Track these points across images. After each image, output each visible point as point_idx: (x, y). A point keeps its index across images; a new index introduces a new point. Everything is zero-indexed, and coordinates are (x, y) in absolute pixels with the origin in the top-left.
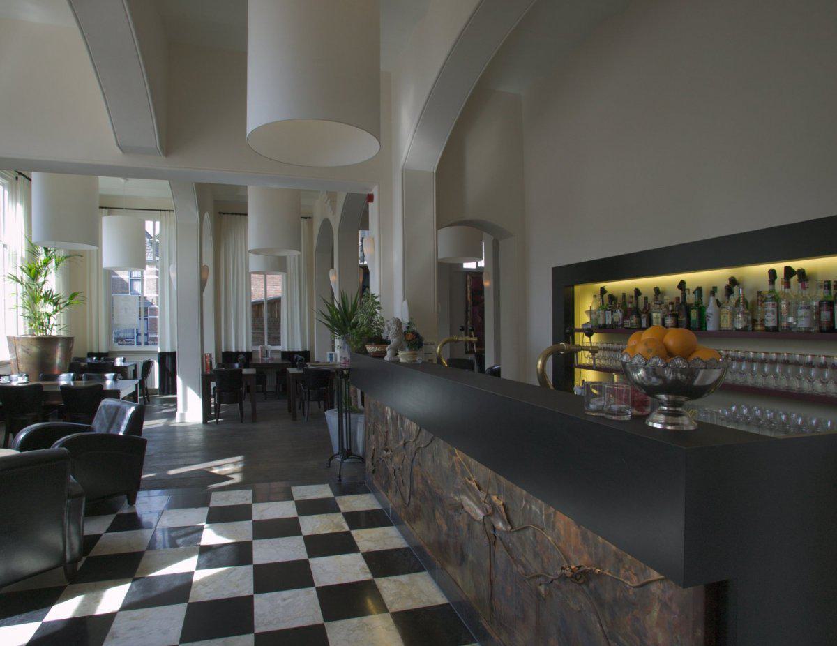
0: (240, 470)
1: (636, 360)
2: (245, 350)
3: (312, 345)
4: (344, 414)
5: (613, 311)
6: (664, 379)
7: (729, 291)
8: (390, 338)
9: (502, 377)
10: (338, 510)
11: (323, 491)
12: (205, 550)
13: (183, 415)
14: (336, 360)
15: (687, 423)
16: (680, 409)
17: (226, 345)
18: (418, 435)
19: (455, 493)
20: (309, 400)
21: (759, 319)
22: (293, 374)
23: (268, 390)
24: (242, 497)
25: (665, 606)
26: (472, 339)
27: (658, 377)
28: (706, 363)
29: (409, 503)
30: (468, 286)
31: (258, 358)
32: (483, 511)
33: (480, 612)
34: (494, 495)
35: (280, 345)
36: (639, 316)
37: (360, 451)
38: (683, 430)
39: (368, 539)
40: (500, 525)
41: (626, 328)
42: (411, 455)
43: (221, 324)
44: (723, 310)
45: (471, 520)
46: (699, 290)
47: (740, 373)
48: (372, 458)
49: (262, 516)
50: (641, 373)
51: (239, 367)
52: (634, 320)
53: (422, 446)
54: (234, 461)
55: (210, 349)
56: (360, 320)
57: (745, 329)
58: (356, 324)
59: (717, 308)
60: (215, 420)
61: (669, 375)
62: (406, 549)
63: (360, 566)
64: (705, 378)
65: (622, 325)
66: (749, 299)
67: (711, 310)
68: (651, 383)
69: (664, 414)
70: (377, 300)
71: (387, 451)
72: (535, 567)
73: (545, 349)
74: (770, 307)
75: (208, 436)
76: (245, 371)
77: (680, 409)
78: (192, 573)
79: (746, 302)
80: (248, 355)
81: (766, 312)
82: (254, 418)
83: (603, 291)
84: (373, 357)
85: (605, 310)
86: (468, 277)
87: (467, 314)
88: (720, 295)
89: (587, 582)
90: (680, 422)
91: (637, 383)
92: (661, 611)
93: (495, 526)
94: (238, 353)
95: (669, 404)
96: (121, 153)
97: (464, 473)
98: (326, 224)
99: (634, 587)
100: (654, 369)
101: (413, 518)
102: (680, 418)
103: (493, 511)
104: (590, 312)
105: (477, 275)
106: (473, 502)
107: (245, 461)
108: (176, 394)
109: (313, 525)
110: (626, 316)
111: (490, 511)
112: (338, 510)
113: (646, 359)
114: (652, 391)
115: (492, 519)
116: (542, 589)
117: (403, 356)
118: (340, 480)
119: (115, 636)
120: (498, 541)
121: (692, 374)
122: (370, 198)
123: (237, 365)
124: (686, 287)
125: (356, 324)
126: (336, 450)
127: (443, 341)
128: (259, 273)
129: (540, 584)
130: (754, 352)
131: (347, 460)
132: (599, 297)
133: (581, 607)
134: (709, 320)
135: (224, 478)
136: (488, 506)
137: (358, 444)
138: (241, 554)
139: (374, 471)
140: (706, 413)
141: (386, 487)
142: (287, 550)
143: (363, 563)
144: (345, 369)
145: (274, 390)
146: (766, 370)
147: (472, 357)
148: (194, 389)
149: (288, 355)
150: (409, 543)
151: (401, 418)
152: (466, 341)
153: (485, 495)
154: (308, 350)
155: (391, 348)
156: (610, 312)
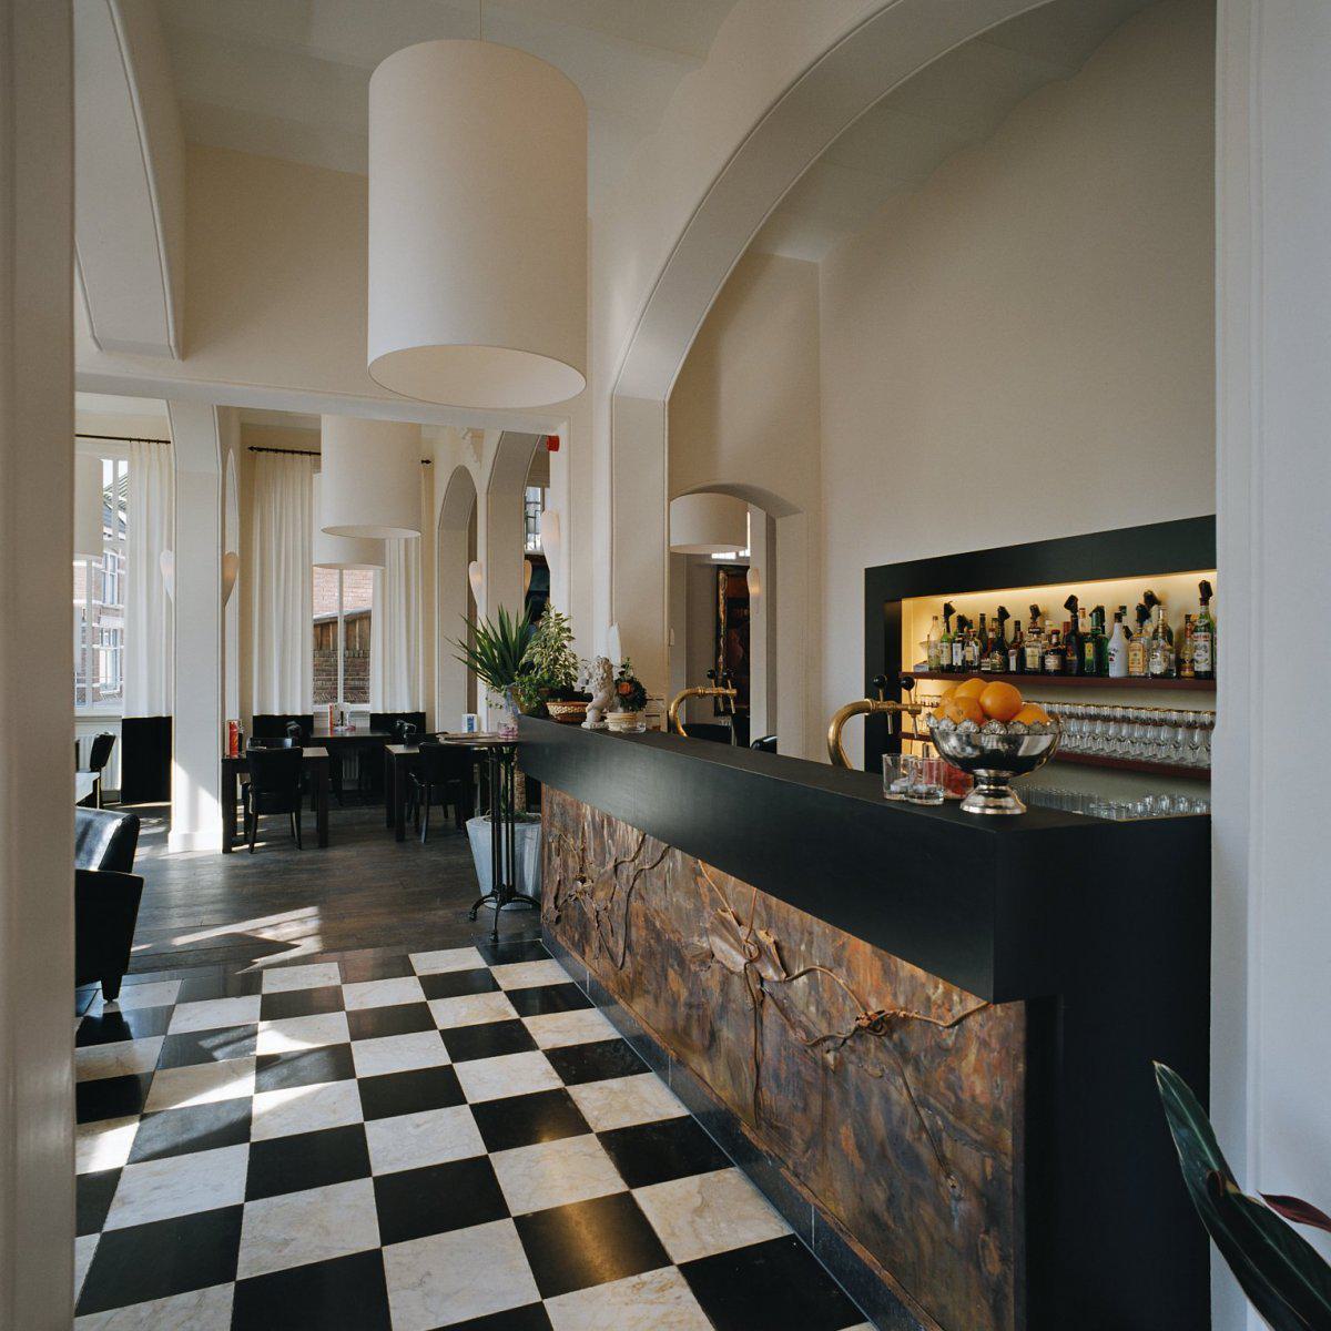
0: (315, 931)
1: (943, 726)
2: (299, 714)
3: (430, 701)
4: (503, 825)
5: (964, 644)
6: (982, 749)
7: (1143, 614)
8: (592, 691)
9: (779, 753)
10: (497, 988)
11: (469, 959)
12: (265, 1064)
13: (188, 838)
14: (479, 727)
15: (1013, 805)
16: (1004, 788)
17: (262, 703)
18: (639, 849)
19: (701, 936)
20: (430, 804)
21: (1187, 658)
22: (397, 755)
23: (346, 787)
24: (323, 975)
25: (984, 1044)
26: (728, 692)
27: (974, 747)
28: (1029, 728)
29: (623, 964)
30: (721, 592)
31: (324, 728)
32: (744, 955)
33: (740, 1115)
34: (761, 929)
35: (366, 701)
36: (1005, 653)
37: (530, 891)
38: (1007, 815)
39: (553, 1030)
40: (770, 973)
41: (985, 672)
42: (628, 882)
43: (252, 666)
44: (1133, 644)
45: (727, 975)
46: (1100, 611)
47: (1145, 744)
48: (556, 898)
49: (362, 1003)
50: (953, 741)
51: (294, 743)
52: (996, 658)
53: (647, 867)
54: (299, 916)
55: (233, 715)
56: (536, 660)
57: (1166, 675)
58: (530, 665)
59: (1125, 640)
60: (247, 846)
61: (991, 743)
62: (618, 1041)
63: (541, 1070)
64: (1032, 746)
65: (979, 667)
66: (1175, 626)
67: (1115, 643)
68: (965, 754)
69: (985, 795)
70: (565, 625)
71: (583, 881)
72: (822, 1029)
73: (841, 708)
74: (1201, 640)
75: (235, 877)
76: (308, 752)
77: (1004, 788)
78: (250, 1099)
79: (1168, 633)
80: (306, 722)
81: (1196, 648)
82: (323, 839)
83: (948, 610)
84: (560, 722)
85: (952, 641)
86: (722, 575)
87: (718, 642)
88: (1130, 619)
89: (889, 1035)
90: (1004, 804)
91: (947, 755)
92: (979, 1051)
93: (763, 975)
94: (285, 719)
95: (989, 781)
96: (96, 349)
97: (715, 902)
98: (462, 476)
99: (948, 1027)
100: (968, 736)
101: (631, 989)
102: (1003, 800)
103: (760, 952)
104: (928, 645)
105: (738, 572)
106: (732, 946)
107: (324, 916)
108: (168, 799)
109: (454, 1012)
110: (984, 653)
111: (755, 954)
112: (497, 988)
113: (955, 723)
114: (968, 765)
115: (758, 965)
116: (830, 1057)
117: (616, 721)
118: (496, 940)
119: (126, 1200)
120: (768, 998)
121: (1014, 741)
122: (553, 443)
123: (289, 742)
124: (1079, 607)
125: (530, 665)
126: (486, 887)
127: (679, 697)
128: (330, 566)
129: (828, 1052)
130: (1195, 712)
131: (507, 907)
132: (942, 619)
133: (883, 1070)
134: (1112, 660)
135: (286, 946)
136: (752, 948)
137: (526, 876)
138: (338, 1063)
139: (558, 919)
140: (1109, 808)
141: (581, 945)
142: (420, 1052)
143: (548, 1066)
144: (507, 744)
145: (356, 788)
146: (1196, 739)
147: (725, 722)
148: (210, 792)
149: (383, 722)
150: (621, 1033)
151: (610, 823)
152: (719, 695)
153: (748, 930)
154: (421, 711)
155: (593, 707)
156: (959, 645)
